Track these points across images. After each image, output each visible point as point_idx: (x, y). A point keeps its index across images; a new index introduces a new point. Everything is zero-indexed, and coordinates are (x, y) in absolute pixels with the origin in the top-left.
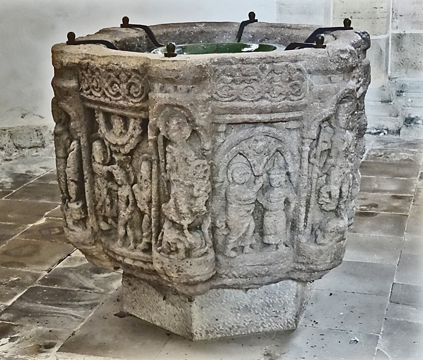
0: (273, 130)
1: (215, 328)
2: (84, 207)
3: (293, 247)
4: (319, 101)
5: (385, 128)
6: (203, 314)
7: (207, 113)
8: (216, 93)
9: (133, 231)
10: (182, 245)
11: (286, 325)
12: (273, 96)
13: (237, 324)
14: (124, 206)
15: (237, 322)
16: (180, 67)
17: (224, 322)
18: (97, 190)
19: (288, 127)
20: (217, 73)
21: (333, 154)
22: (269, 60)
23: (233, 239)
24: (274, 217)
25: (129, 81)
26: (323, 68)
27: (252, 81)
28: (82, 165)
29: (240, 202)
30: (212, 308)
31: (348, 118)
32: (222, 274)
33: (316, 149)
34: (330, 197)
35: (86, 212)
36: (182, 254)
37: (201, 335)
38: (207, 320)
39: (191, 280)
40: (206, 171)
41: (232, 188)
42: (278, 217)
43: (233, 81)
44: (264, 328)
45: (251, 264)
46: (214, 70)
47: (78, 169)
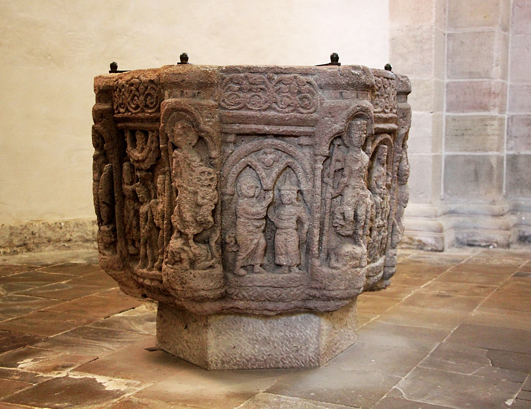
0: (284, 144)
1: (231, 359)
2: (114, 230)
3: (308, 271)
4: (330, 116)
5: (494, 241)
6: (219, 342)
7: (213, 120)
8: (223, 101)
9: (152, 250)
10: (186, 255)
11: (307, 362)
12: (281, 106)
13: (254, 356)
14: (143, 223)
15: (256, 354)
16: (185, 71)
17: (241, 354)
18: (125, 212)
19: (300, 143)
20: (224, 81)
21: (346, 172)
22: (277, 70)
23: (242, 255)
24: (285, 236)
25: (146, 92)
26: (333, 82)
27: (259, 90)
28: (113, 186)
29: (248, 216)
30: (228, 336)
31: (361, 136)
32: (232, 294)
33: (330, 168)
34: (344, 218)
35: (116, 236)
36: (186, 264)
37: (217, 365)
38: (224, 349)
39: (196, 294)
40: (212, 180)
41: (241, 201)
42: (289, 236)
43: (240, 89)
44: (284, 363)
45: (260, 284)
46: (222, 78)
47: (110, 191)
